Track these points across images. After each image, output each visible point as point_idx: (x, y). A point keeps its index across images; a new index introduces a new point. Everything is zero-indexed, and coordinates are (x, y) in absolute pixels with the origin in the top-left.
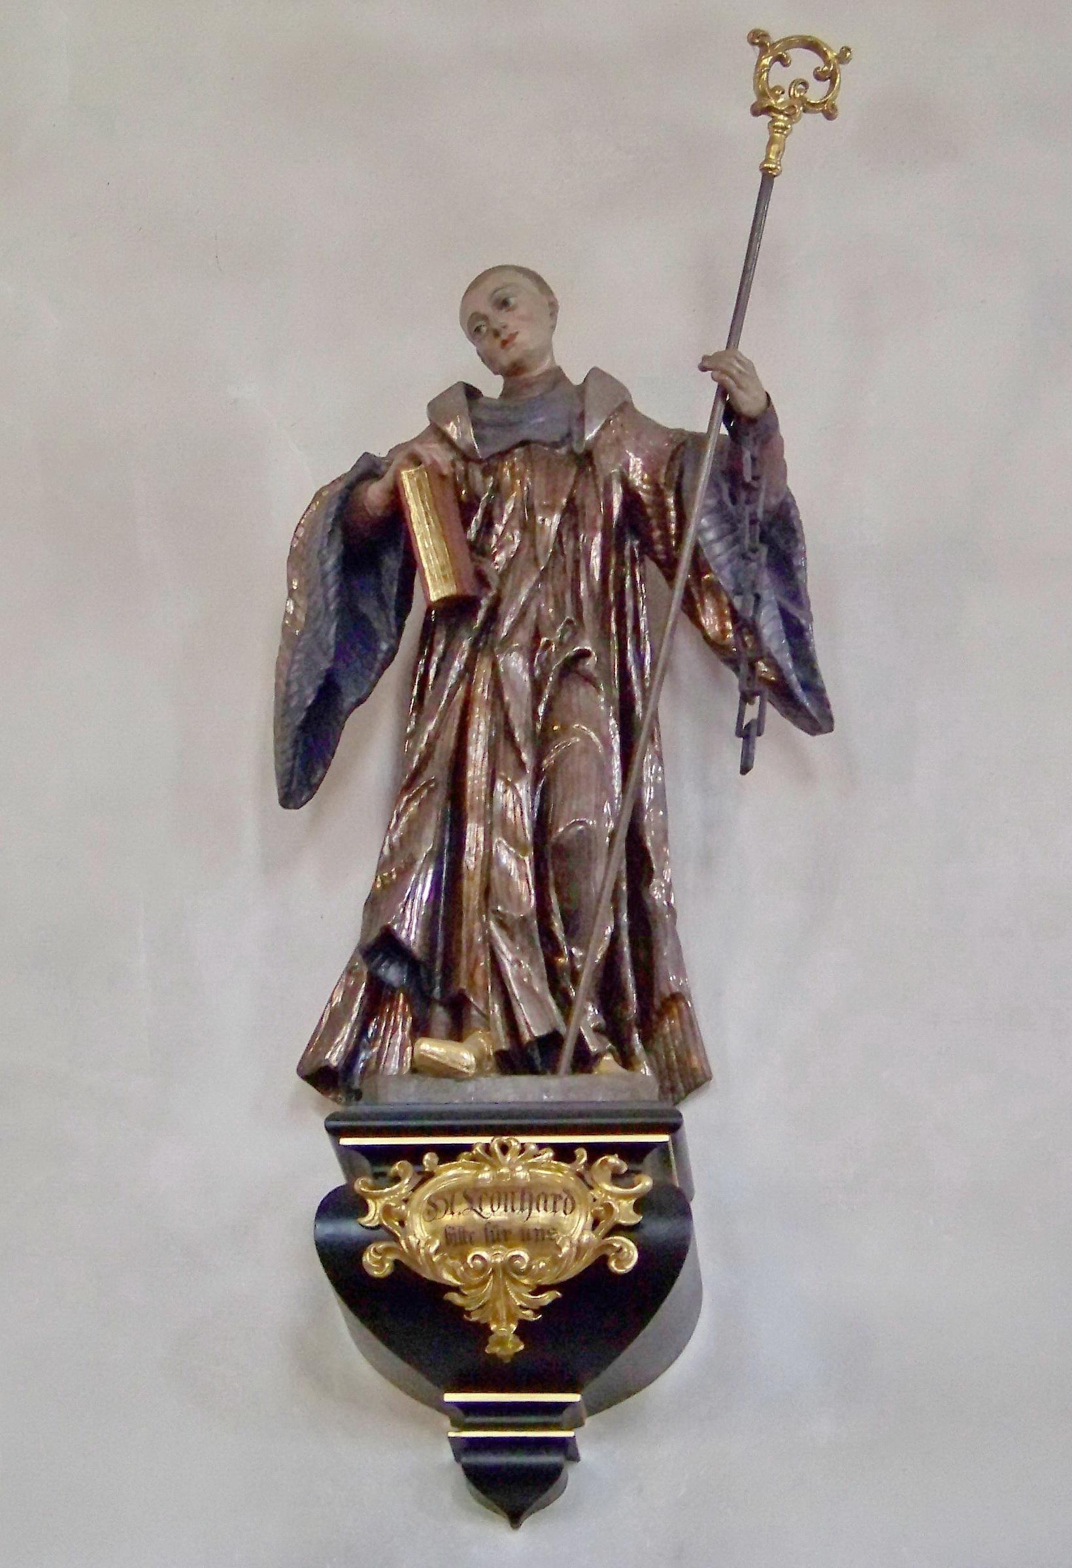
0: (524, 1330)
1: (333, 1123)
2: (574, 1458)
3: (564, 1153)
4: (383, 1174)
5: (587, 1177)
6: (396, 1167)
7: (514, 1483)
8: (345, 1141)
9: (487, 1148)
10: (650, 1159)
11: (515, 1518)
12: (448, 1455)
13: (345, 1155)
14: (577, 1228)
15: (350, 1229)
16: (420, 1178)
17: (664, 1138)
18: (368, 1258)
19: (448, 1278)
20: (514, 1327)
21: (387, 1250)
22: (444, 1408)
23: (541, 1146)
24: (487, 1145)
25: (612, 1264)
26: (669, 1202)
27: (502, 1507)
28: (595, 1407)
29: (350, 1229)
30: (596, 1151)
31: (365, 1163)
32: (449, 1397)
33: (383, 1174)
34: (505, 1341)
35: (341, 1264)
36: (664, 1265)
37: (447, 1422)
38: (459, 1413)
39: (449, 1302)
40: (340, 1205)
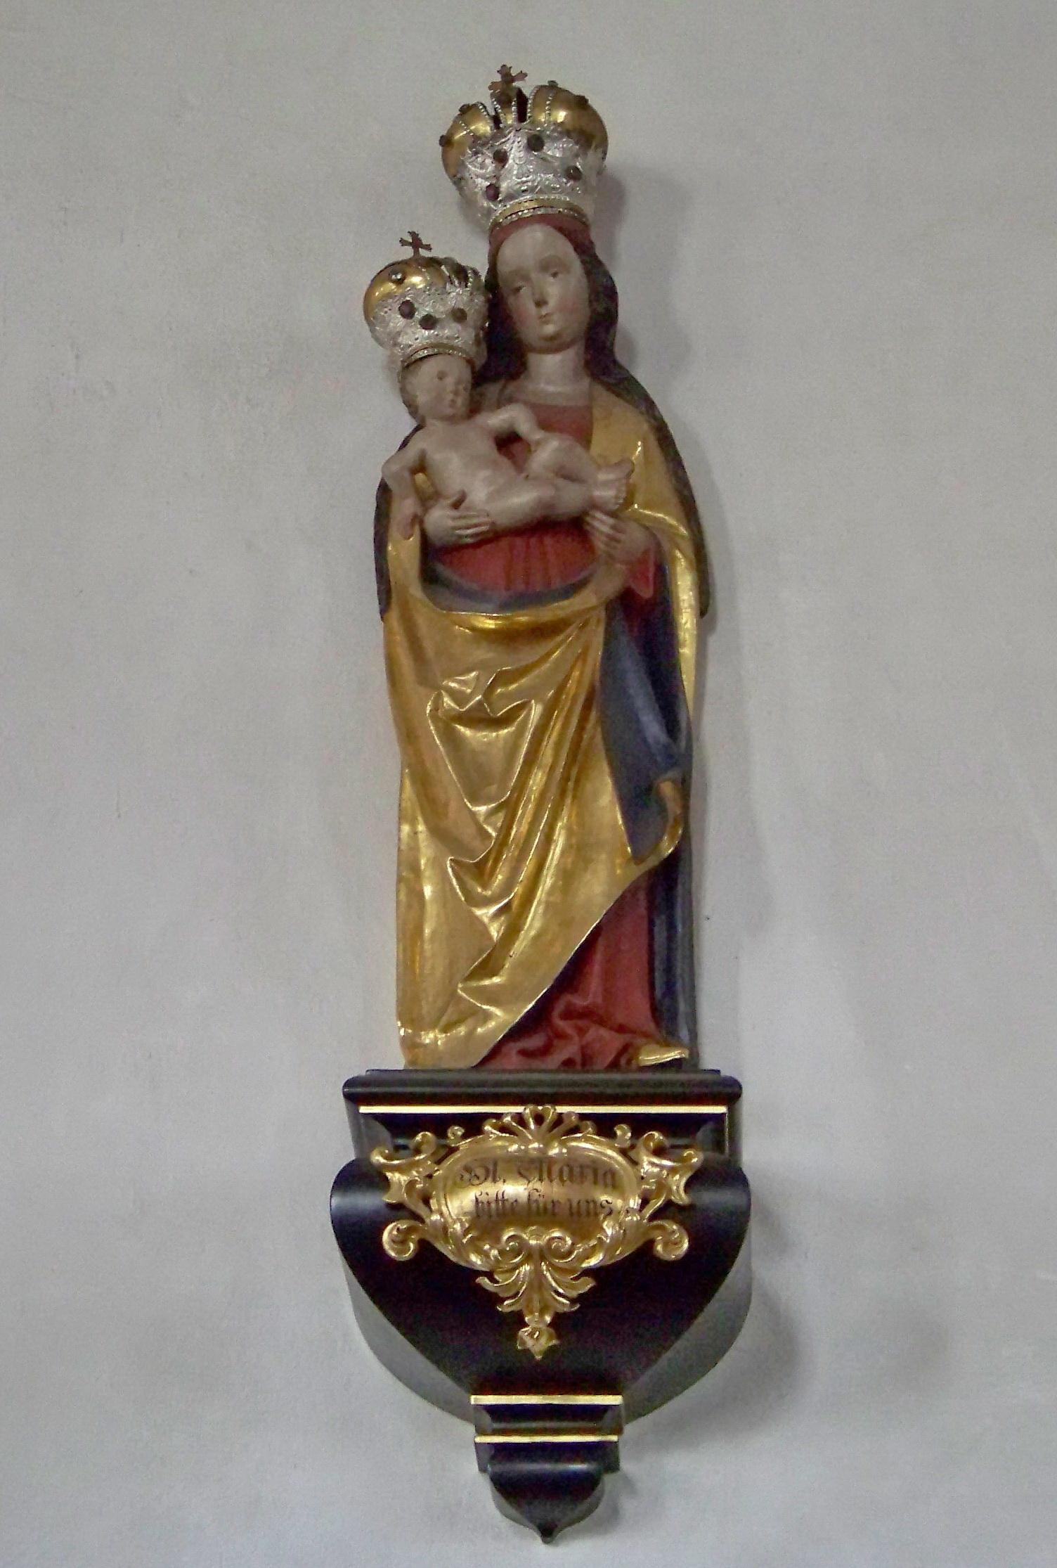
0: (560, 1323)
1: (353, 1090)
2: (613, 1467)
3: (605, 1126)
4: (405, 1147)
5: (632, 1154)
6: (419, 1137)
7: (549, 1491)
8: (364, 1109)
9: (520, 1119)
10: (703, 1133)
11: (548, 1532)
12: (470, 1467)
13: (362, 1127)
14: (634, 1191)
15: (366, 1201)
16: (443, 1152)
17: (721, 1109)
18: (387, 1235)
19: (475, 1259)
20: (548, 1319)
21: (410, 1230)
22: (462, 1412)
23: (583, 1117)
24: (519, 1114)
25: (659, 1248)
26: (724, 1172)
27: (531, 1519)
28: (636, 1410)
29: (366, 1201)
30: (640, 1125)
31: (384, 1133)
32: (474, 1399)
33: (405, 1147)
34: (536, 1338)
35: (357, 1240)
36: (718, 1244)
37: (471, 1429)
38: (487, 1419)
39: (479, 1287)
40: (355, 1177)
